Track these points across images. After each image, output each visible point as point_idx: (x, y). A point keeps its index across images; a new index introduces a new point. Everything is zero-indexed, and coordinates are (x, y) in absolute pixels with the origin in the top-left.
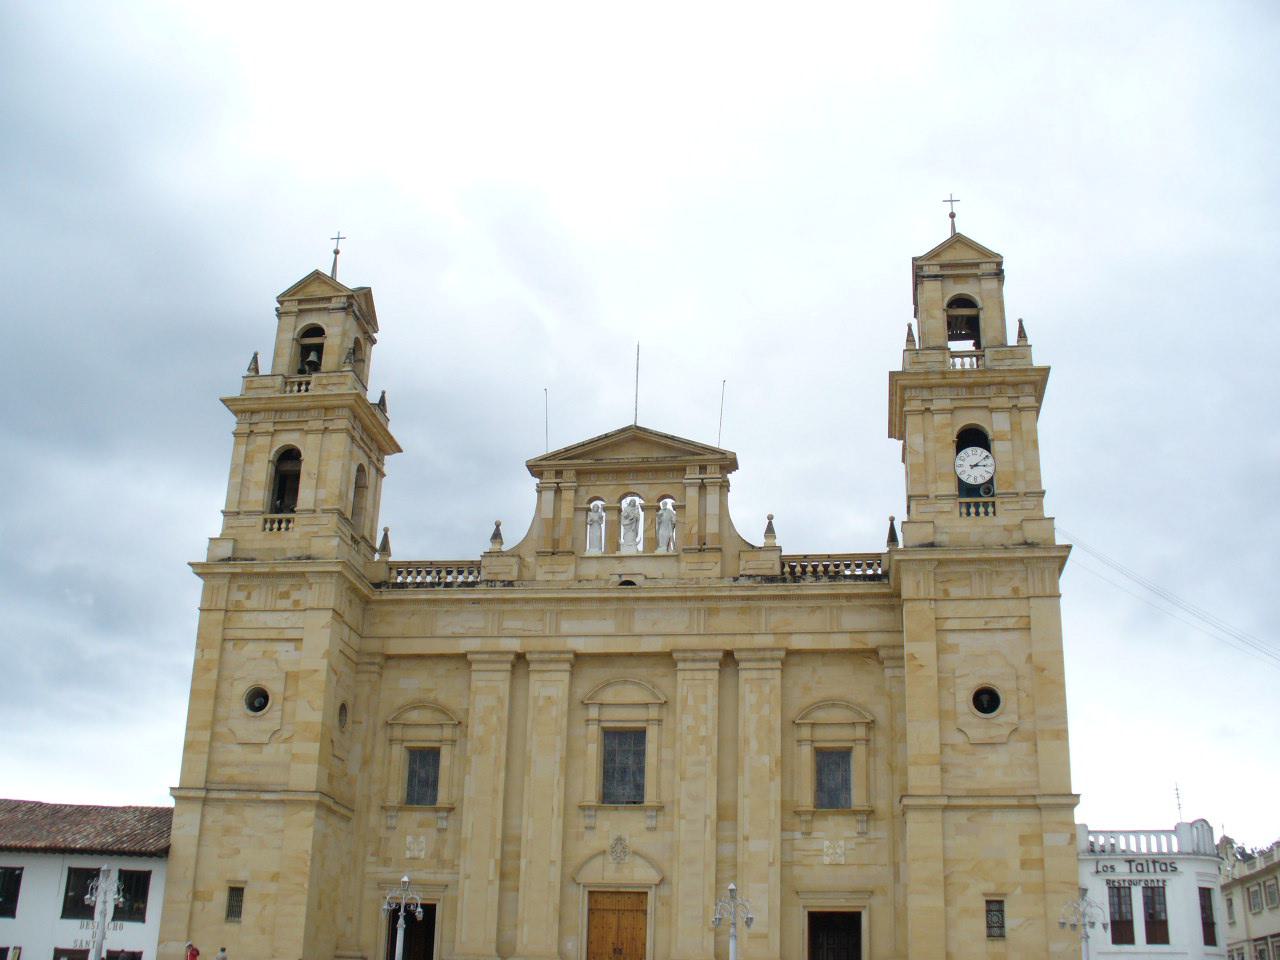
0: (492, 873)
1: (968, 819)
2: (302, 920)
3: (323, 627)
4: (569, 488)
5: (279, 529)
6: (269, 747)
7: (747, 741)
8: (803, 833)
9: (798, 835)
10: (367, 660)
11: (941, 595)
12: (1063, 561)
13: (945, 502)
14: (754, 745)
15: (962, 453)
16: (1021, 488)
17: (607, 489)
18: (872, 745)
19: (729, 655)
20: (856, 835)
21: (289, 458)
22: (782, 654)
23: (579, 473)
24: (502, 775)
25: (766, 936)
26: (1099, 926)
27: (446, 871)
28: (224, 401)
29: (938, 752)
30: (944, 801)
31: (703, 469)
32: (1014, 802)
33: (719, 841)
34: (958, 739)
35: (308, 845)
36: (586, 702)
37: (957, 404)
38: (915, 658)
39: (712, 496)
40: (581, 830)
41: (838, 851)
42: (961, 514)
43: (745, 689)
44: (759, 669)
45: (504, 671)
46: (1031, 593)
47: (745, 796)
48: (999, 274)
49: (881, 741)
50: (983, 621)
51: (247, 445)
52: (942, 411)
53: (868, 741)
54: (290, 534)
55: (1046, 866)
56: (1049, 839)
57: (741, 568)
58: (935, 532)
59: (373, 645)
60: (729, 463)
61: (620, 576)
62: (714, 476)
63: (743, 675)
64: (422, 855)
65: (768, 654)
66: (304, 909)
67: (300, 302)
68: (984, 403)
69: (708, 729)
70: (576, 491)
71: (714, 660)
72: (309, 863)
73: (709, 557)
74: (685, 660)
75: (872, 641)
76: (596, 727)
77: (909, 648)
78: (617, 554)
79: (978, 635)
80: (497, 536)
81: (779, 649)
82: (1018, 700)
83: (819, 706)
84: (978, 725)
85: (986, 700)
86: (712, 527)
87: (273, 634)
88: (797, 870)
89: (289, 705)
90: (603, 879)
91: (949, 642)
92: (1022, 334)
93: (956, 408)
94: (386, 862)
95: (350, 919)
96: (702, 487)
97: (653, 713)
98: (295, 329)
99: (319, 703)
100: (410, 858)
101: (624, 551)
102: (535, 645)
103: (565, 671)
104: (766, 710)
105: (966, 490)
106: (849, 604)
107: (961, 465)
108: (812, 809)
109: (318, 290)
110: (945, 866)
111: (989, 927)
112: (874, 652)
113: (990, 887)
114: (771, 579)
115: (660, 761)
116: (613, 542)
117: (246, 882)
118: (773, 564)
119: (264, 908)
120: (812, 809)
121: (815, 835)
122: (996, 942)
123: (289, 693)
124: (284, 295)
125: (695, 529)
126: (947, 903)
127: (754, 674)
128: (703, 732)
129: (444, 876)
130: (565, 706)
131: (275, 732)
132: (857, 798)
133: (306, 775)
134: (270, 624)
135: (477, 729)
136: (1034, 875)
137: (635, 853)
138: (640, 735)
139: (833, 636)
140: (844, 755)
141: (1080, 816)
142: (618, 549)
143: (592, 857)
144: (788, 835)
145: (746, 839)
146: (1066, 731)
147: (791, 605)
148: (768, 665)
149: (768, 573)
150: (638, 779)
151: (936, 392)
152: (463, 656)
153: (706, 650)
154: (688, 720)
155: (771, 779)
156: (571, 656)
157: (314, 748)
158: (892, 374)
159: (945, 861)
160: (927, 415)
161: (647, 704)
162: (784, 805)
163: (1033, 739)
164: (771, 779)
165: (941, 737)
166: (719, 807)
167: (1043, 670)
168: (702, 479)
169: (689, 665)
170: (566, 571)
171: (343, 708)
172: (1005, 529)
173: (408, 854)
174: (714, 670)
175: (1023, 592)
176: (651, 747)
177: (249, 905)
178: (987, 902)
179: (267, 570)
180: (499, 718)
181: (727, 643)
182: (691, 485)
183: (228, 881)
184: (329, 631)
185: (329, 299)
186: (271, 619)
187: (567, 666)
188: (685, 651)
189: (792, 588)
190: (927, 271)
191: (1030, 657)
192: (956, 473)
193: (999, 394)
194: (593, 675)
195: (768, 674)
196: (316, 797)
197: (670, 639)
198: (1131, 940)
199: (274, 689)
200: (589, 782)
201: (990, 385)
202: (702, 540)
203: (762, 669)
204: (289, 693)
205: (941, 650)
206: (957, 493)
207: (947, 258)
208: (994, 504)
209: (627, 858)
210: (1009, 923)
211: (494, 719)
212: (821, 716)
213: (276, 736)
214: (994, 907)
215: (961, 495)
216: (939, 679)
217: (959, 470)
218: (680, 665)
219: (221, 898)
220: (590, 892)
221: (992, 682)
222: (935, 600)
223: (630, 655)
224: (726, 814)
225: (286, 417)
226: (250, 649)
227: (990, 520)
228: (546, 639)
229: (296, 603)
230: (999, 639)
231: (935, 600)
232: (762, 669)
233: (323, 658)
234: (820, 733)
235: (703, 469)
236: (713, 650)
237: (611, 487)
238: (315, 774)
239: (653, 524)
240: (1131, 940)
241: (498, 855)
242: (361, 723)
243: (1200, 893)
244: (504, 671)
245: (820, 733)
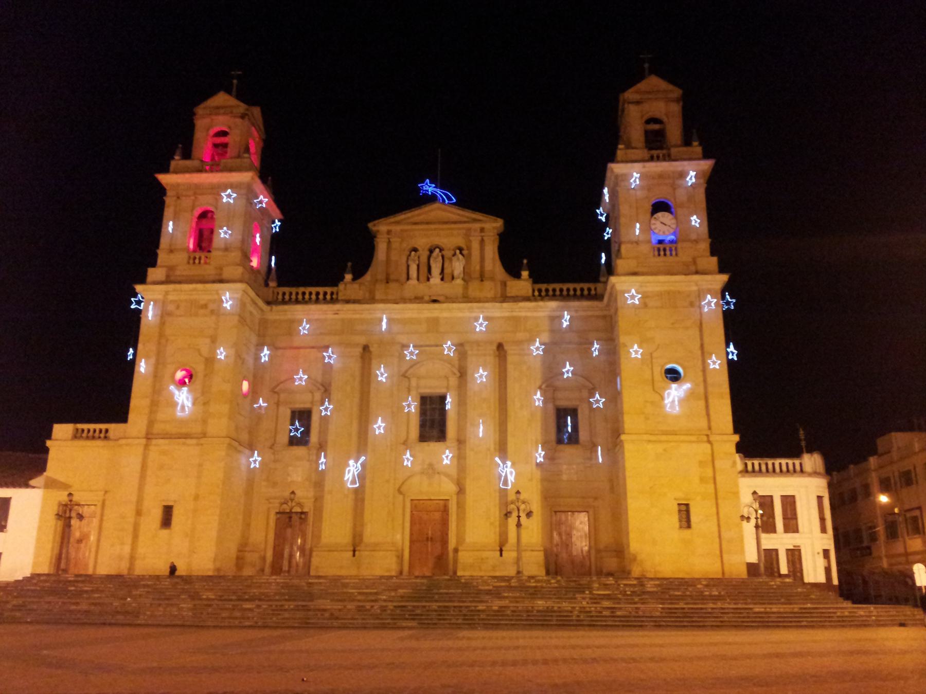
1: (665, 450)
15: (655, 216)
54: (207, 267)
61: (430, 296)
64: (299, 479)
72: (221, 486)
107: (654, 224)
113: (680, 495)
117: (175, 501)
179: (375, 591)
183: (164, 500)
196: (228, 440)
198: (774, 530)
208: (676, 249)
219: (157, 514)
228: (421, 266)
240: (774, 530)
243: (781, 499)
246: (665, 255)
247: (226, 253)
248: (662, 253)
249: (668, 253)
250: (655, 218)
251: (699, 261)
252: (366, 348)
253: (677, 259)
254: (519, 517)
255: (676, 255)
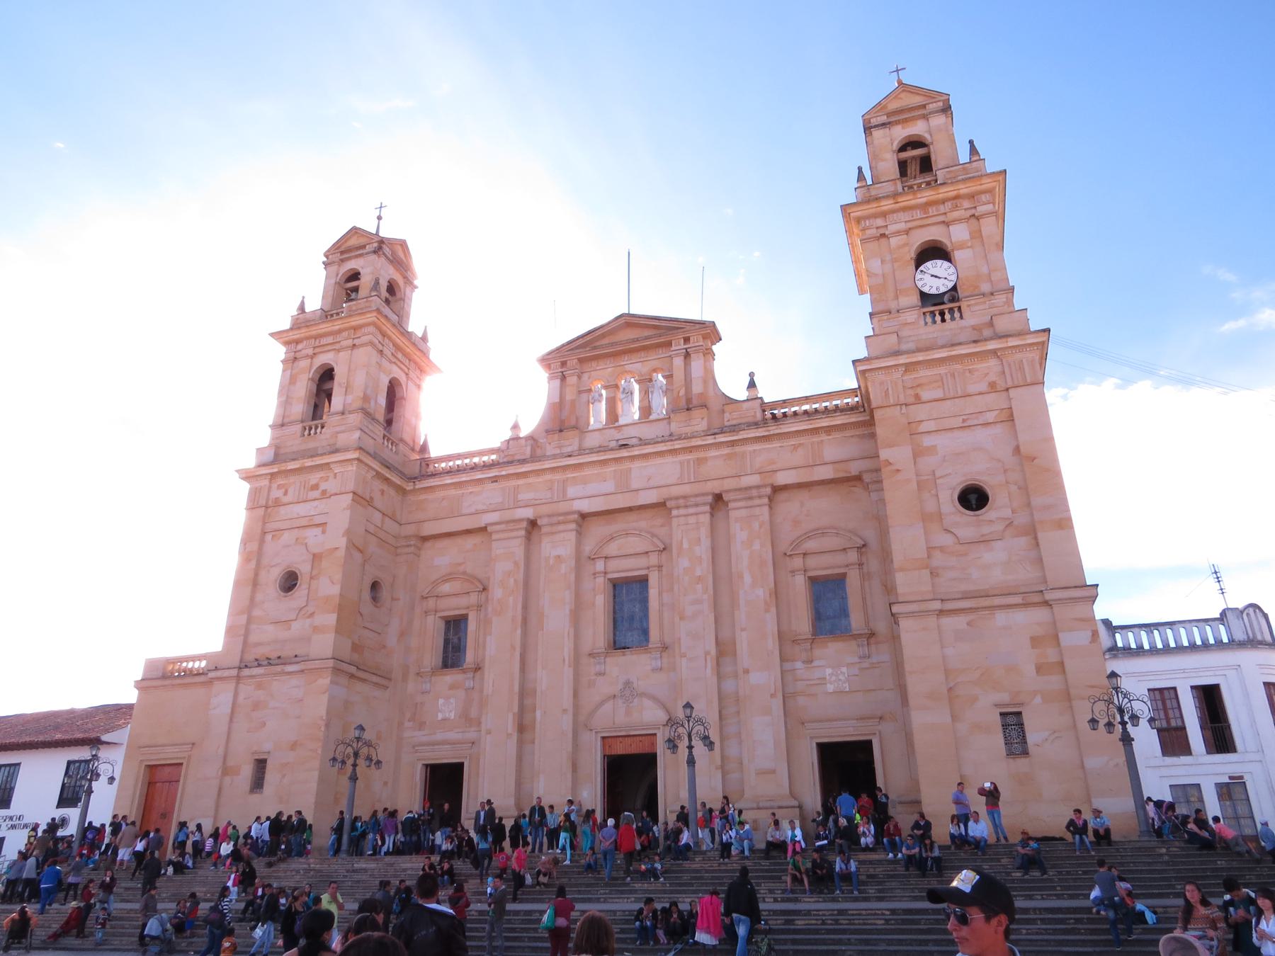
0: (511, 726)
1: (969, 624)
2: (313, 786)
3: (344, 509)
4: (573, 375)
5: (316, 433)
6: (295, 622)
7: (741, 577)
8: (803, 662)
9: (799, 665)
10: (405, 544)
11: (912, 400)
12: (1043, 348)
13: (908, 314)
14: (747, 579)
15: (922, 268)
16: (986, 287)
17: (605, 369)
18: (865, 569)
19: (718, 498)
20: (856, 659)
21: (327, 375)
22: (768, 490)
23: (581, 361)
24: (519, 631)
25: (773, 772)
26: (1143, 723)
27: (473, 729)
28: (272, 335)
29: (926, 556)
30: (937, 605)
31: (687, 340)
32: (1017, 599)
33: (720, 677)
34: (947, 540)
35: (323, 712)
36: (593, 557)
37: (910, 225)
38: (891, 464)
39: (697, 364)
40: (592, 678)
41: (841, 677)
42: (926, 323)
43: (736, 528)
44: (747, 507)
45: (518, 537)
46: (1010, 384)
47: (743, 630)
48: (946, 109)
49: (873, 565)
50: (961, 418)
51: (292, 369)
52: (898, 233)
53: (861, 565)
54: (322, 437)
55: (1067, 670)
56: (1067, 639)
57: (726, 420)
58: (899, 343)
59: (410, 530)
60: (709, 332)
61: (617, 440)
62: (697, 344)
63: (733, 514)
64: (452, 715)
65: (754, 493)
66: (316, 774)
67: (342, 253)
68: (941, 218)
69: (703, 569)
70: (579, 377)
71: (705, 504)
72: (323, 729)
73: (696, 413)
74: (678, 508)
75: (854, 468)
76: (602, 578)
77: (884, 454)
78: (617, 424)
79: (957, 433)
80: (515, 427)
81: (765, 486)
82: (1009, 493)
83: (809, 536)
84: (966, 523)
85: (974, 498)
86: (697, 388)
87: (304, 522)
88: (801, 701)
89: (314, 582)
90: (614, 724)
91: (925, 445)
92: (973, 150)
93: (910, 229)
94: (421, 726)
95: (386, 783)
96: (687, 355)
97: (654, 559)
98: (337, 275)
99: (338, 576)
100: (442, 720)
101: (622, 421)
102: (729, 484)
103: (571, 530)
104: (757, 546)
105: (925, 297)
106: (830, 437)
108: (810, 636)
109: (353, 242)
110: (947, 678)
111: (1008, 743)
112: (858, 478)
113: (1004, 697)
114: (756, 425)
115: (661, 605)
116: (613, 415)
118: (755, 412)
119: (284, 776)
120: (810, 636)
121: (816, 663)
122: (1018, 760)
123: (314, 573)
124: (328, 251)
125: (682, 392)
126: (954, 718)
127: (743, 513)
128: (698, 573)
129: (471, 735)
130: (573, 563)
131: (301, 609)
132: (856, 621)
133: (324, 645)
134: (302, 514)
135: (497, 593)
136: (1054, 681)
137: (643, 695)
138: (643, 581)
139: (815, 468)
140: (840, 580)
141: (1102, 609)
142: (617, 420)
143: (602, 703)
144: (788, 666)
145: (746, 671)
146: (1069, 519)
147: (774, 445)
148: (757, 502)
149: (751, 420)
150: (645, 624)
151: (890, 217)
152: (483, 530)
153: (697, 496)
154: (684, 563)
155: (767, 611)
156: (576, 516)
157: (331, 619)
158: (845, 208)
159: (947, 672)
160: (883, 240)
161: (647, 553)
162: (781, 636)
163: (1031, 531)
164: (767, 611)
165: (927, 541)
166: (717, 643)
167: (1033, 459)
168: (686, 349)
169: (682, 511)
170: (571, 443)
171: (375, 586)
172: (974, 329)
173: (440, 716)
174: (705, 513)
175: (1001, 384)
176: (653, 592)
177: (271, 777)
178: (1001, 714)
180: (515, 581)
181: (715, 487)
182: (677, 355)
183: (255, 753)
184: (349, 511)
185: (364, 247)
186: (301, 509)
187: (573, 526)
188: (677, 498)
189: (774, 429)
190: (874, 122)
191: (1017, 450)
192: (955, 267)
193: (956, 208)
194: (598, 531)
195: (757, 511)
197: (664, 490)
198: (1185, 749)
199: (304, 569)
200: (597, 628)
201: (943, 202)
202: (689, 400)
203: (751, 507)
204: (314, 573)
205: (917, 454)
206: (920, 304)
207: (893, 106)
208: (959, 308)
209: (636, 700)
210: (1032, 738)
211: (512, 580)
212: (811, 545)
213: (303, 612)
214: (1011, 720)
215: (923, 305)
216: (919, 483)
217: (919, 284)
218: (675, 512)
219: (247, 771)
220: (603, 738)
221: (984, 478)
222: (906, 405)
223: (630, 509)
224: (724, 650)
225: (324, 341)
226: (287, 537)
227: (958, 323)
229: (324, 492)
230: (981, 436)
231: (906, 405)
232: (751, 507)
233: (343, 536)
234: (812, 562)
235: (687, 340)
236: (703, 495)
237: (610, 369)
238: (332, 644)
239: (645, 393)
240: (1185, 749)
241: (516, 709)
242: (399, 599)
244: (518, 537)
245: (812, 562)
246: (943, 320)
247: (343, 417)
248: (938, 318)
249: (947, 316)
250: (922, 271)
251: (997, 321)
252: (533, 524)
253: (963, 323)
254: (690, 747)
255: (961, 317)
